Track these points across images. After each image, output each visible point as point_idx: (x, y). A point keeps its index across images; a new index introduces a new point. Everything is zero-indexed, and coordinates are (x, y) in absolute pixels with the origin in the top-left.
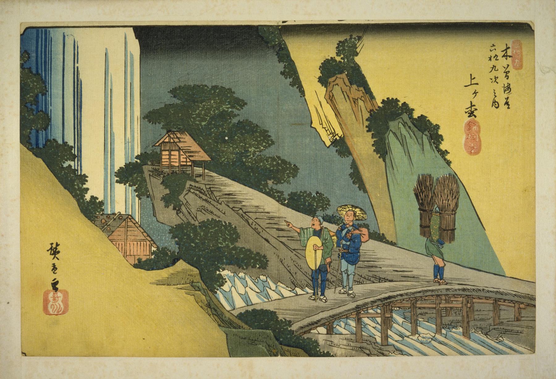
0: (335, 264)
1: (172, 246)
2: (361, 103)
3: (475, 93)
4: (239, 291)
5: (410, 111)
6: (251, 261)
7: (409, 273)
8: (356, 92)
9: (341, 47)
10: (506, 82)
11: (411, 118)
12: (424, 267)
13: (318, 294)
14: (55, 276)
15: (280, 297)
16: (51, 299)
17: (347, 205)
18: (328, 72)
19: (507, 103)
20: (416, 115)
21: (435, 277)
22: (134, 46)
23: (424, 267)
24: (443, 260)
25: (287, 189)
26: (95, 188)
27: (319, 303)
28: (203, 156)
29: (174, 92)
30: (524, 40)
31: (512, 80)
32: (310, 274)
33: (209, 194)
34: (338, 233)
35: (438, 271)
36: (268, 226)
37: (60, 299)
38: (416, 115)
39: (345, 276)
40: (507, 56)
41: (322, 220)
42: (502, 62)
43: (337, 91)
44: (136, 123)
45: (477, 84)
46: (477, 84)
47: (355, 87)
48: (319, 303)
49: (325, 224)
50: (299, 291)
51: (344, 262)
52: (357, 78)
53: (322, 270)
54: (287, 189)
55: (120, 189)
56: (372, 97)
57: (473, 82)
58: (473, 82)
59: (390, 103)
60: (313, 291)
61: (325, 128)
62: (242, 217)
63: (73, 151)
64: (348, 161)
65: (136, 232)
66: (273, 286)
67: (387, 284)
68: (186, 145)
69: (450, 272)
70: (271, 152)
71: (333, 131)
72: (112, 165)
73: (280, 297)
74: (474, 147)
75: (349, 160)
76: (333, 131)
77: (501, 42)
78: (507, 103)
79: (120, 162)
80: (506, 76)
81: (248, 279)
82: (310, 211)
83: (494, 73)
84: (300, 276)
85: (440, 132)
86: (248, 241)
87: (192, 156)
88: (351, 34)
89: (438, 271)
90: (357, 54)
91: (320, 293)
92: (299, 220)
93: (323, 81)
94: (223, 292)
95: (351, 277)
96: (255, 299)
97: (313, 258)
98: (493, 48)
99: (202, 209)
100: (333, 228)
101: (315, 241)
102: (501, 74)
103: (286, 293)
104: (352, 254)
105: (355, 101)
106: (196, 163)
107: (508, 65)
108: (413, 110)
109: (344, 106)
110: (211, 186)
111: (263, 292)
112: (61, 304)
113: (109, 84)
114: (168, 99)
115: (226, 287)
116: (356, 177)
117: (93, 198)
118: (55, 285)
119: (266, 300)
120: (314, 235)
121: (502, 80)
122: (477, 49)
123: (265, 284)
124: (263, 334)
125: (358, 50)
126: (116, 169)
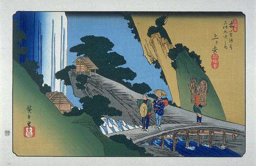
0: (152, 115)
1: (80, 107)
2: (166, 45)
3: (217, 42)
4: (110, 127)
5: (187, 50)
6: (115, 113)
7: (187, 120)
8: (163, 40)
9: (157, 22)
10: (231, 38)
11: (188, 52)
12: (193, 117)
13: (144, 128)
14: (29, 120)
15: (128, 129)
16: (27, 131)
17: (158, 90)
18: (151, 31)
19: (231, 47)
20: (190, 51)
21: (198, 122)
22: (65, 18)
23: (193, 117)
24: (201, 114)
25: (132, 82)
26: (47, 81)
27: (145, 132)
28: (95, 67)
29: (82, 39)
30: (239, 19)
31: (233, 38)
32: (142, 119)
33: (97, 84)
34: (155, 102)
35: (199, 119)
36: (123, 98)
37: (31, 130)
38: (190, 51)
39: (157, 120)
40: (231, 27)
41: (147, 96)
42: (229, 29)
43: (155, 40)
44: (65, 53)
45: (218, 38)
46: (218, 38)
47: (163, 38)
48: (145, 132)
49: (149, 98)
50: (136, 127)
51: (157, 115)
52: (164, 35)
53: (147, 118)
54: (132, 82)
55: (58, 82)
56: (170, 43)
57: (216, 37)
58: (216, 37)
59: (179, 46)
60: (143, 127)
61: (149, 56)
62: (112, 94)
63: (38, 64)
64: (159, 71)
65: (65, 100)
66: (125, 124)
67: (177, 125)
68: (88, 62)
69: (205, 119)
70: (124, 66)
71: (153, 58)
72: (55, 69)
73: (128, 129)
74: (215, 64)
75: (159, 71)
76: (153, 58)
77: (229, 20)
78: (231, 47)
79: (58, 69)
80: (230, 35)
81: (114, 120)
82: (142, 93)
83: (226, 34)
84: (137, 120)
85: (200, 59)
86: (114, 104)
87: (91, 67)
88: (162, 17)
89: (199, 119)
90: (164, 24)
91: (145, 128)
92: (136, 96)
93: (149, 35)
94: (103, 127)
95: (160, 121)
96: (117, 129)
97: (143, 111)
98: (226, 23)
99: (94, 90)
100: (152, 100)
101: (144, 105)
102: (228, 34)
103: (131, 127)
104: (161, 112)
105: (163, 45)
106: (93, 71)
107: (232, 31)
108: (199, 56)
109: (158, 46)
110: (99, 80)
111: (120, 127)
112: (31, 132)
113: (54, 36)
114: (81, 42)
115: (104, 125)
116: (163, 76)
117: (46, 85)
118: (29, 124)
119: (122, 131)
120: (144, 102)
121: (229, 37)
122: (219, 23)
123: (122, 123)
124: (122, 146)
125: (165, 23)
126: (56, 72)
